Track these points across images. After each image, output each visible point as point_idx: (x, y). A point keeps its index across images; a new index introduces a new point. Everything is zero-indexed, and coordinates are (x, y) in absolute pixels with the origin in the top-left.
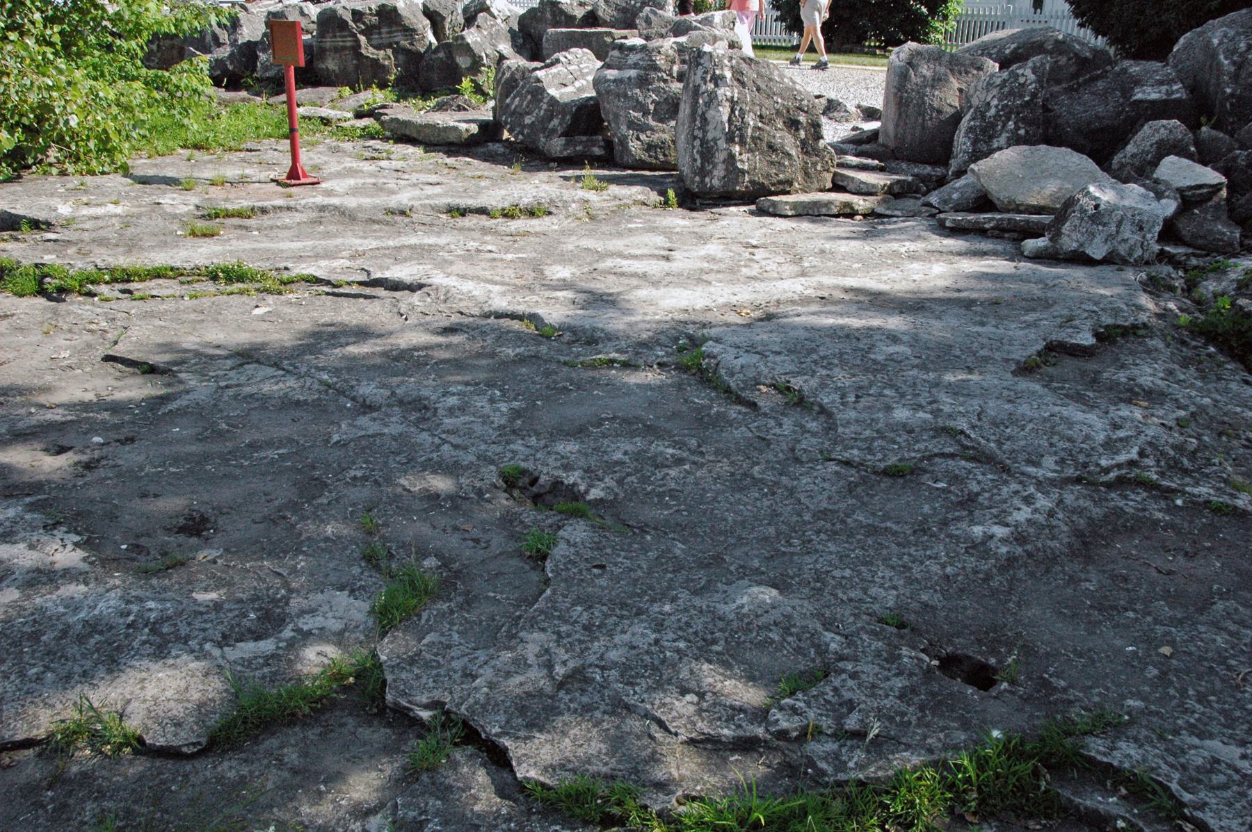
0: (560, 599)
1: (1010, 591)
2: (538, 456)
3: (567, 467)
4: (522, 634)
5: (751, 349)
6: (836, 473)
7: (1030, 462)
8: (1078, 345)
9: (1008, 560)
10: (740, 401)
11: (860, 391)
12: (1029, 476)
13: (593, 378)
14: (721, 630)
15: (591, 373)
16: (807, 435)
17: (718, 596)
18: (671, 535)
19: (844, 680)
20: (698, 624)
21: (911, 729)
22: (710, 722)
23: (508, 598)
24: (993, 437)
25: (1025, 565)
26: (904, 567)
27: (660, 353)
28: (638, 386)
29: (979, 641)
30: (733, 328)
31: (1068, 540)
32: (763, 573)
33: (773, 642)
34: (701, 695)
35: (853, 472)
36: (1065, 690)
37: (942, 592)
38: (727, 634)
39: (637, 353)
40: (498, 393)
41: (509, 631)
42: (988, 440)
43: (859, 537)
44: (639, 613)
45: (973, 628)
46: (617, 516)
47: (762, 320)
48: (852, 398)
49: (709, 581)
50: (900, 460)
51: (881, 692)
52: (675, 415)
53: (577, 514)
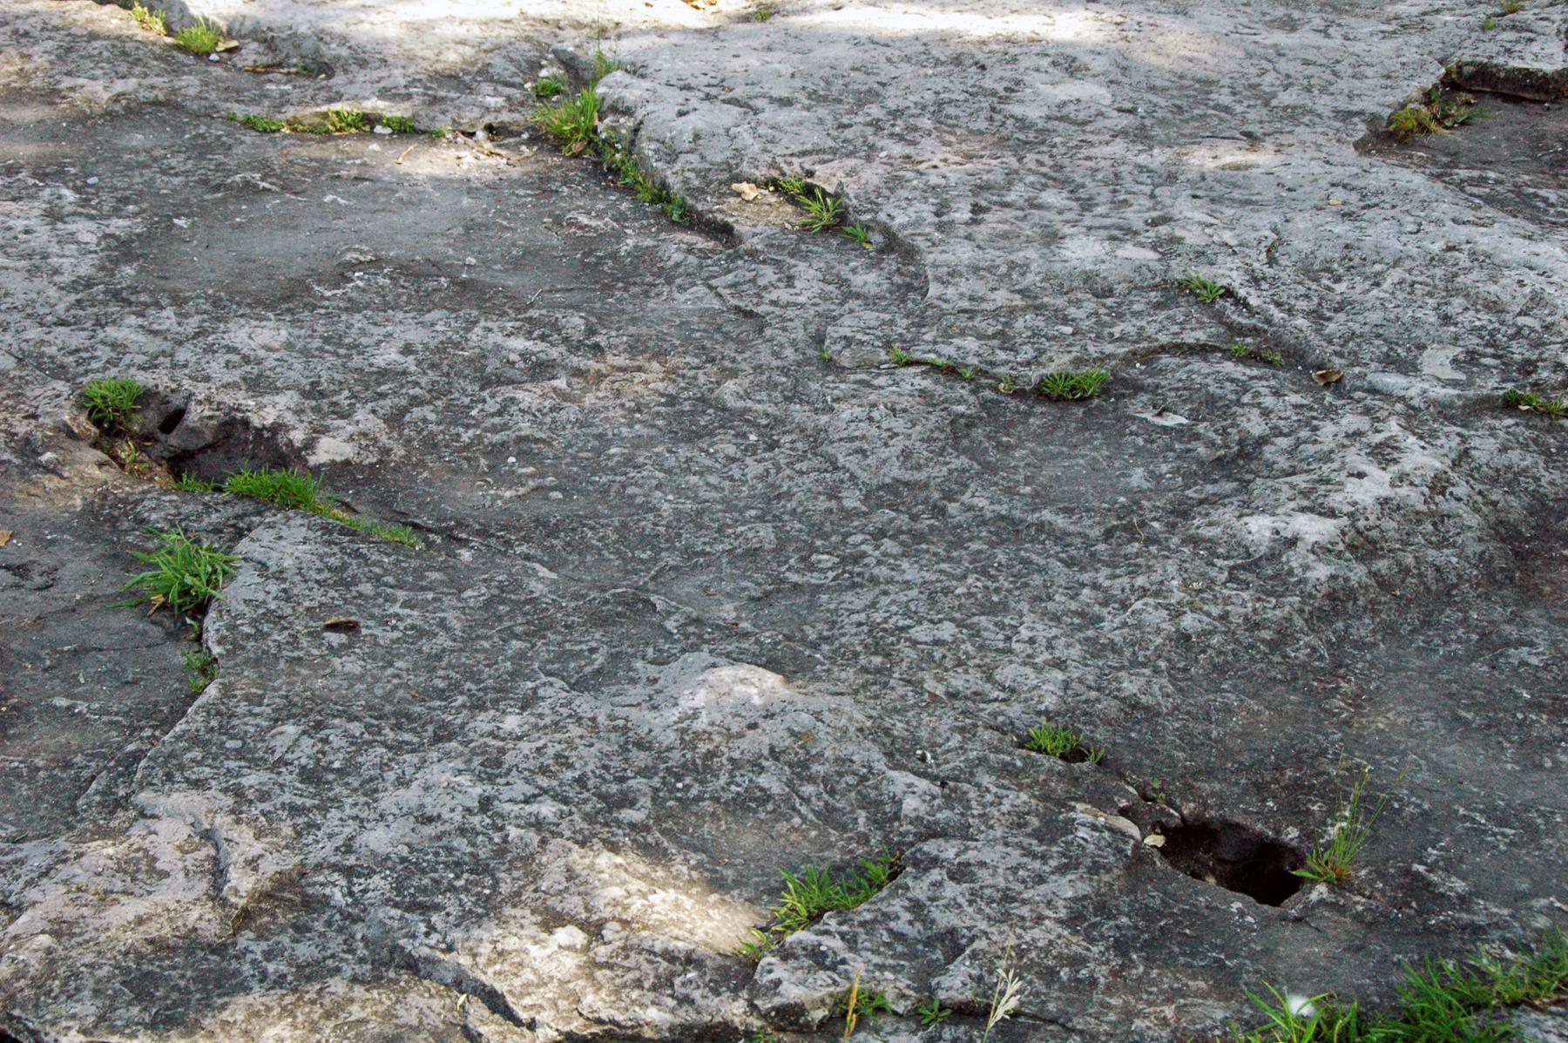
0: (243, 708)
1: (1338, 666)
2: (182, 355)
3: (258, 385)
4: (144, 797)
5: (718, 91)
6: (923, 393)
7: (1391, 362)
8: (1528, 73)
9: (1331, 596)
10: (692, 221)
11: (982, 199)
12: (1387, 396)
13: (323, 162)
14: (645, 772)
15: (314, 150)
16: (853, 304)
17: (636, 693)
18: (524, 548)
19: (937, 884)
20: (587, 759)
21: (1097, 997)
22: (617, 992)
23: (103, 712)
24: (1302, 304)
25: (1373, 608)
26: (1082, 614)
27: (493, 101)
28: (439, 183)
29: (1260, 789)
30: (675, 39)
31: (1479, 548)
32: (746, 635)
33: (766, 797)
34: (595, 930)
35: (962, 391)
36: (1464, 901)
37: (1173, 674)
38: (656, 782)
39: (435, 100)
40: (69, 195)
41: (107, 792)
42: (1290, 311)
43: (974, 546)
44: (443, 734)
45: (1245, 758)
46: (384, 503)
47: (746, 19)
48: (962, 213)
49: (614, 657)
50: (1078, 362)
51: (1025, 911)
52: (530, 257)
53: (292, 502)
